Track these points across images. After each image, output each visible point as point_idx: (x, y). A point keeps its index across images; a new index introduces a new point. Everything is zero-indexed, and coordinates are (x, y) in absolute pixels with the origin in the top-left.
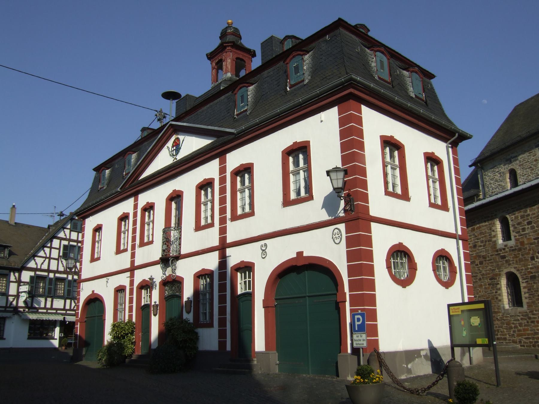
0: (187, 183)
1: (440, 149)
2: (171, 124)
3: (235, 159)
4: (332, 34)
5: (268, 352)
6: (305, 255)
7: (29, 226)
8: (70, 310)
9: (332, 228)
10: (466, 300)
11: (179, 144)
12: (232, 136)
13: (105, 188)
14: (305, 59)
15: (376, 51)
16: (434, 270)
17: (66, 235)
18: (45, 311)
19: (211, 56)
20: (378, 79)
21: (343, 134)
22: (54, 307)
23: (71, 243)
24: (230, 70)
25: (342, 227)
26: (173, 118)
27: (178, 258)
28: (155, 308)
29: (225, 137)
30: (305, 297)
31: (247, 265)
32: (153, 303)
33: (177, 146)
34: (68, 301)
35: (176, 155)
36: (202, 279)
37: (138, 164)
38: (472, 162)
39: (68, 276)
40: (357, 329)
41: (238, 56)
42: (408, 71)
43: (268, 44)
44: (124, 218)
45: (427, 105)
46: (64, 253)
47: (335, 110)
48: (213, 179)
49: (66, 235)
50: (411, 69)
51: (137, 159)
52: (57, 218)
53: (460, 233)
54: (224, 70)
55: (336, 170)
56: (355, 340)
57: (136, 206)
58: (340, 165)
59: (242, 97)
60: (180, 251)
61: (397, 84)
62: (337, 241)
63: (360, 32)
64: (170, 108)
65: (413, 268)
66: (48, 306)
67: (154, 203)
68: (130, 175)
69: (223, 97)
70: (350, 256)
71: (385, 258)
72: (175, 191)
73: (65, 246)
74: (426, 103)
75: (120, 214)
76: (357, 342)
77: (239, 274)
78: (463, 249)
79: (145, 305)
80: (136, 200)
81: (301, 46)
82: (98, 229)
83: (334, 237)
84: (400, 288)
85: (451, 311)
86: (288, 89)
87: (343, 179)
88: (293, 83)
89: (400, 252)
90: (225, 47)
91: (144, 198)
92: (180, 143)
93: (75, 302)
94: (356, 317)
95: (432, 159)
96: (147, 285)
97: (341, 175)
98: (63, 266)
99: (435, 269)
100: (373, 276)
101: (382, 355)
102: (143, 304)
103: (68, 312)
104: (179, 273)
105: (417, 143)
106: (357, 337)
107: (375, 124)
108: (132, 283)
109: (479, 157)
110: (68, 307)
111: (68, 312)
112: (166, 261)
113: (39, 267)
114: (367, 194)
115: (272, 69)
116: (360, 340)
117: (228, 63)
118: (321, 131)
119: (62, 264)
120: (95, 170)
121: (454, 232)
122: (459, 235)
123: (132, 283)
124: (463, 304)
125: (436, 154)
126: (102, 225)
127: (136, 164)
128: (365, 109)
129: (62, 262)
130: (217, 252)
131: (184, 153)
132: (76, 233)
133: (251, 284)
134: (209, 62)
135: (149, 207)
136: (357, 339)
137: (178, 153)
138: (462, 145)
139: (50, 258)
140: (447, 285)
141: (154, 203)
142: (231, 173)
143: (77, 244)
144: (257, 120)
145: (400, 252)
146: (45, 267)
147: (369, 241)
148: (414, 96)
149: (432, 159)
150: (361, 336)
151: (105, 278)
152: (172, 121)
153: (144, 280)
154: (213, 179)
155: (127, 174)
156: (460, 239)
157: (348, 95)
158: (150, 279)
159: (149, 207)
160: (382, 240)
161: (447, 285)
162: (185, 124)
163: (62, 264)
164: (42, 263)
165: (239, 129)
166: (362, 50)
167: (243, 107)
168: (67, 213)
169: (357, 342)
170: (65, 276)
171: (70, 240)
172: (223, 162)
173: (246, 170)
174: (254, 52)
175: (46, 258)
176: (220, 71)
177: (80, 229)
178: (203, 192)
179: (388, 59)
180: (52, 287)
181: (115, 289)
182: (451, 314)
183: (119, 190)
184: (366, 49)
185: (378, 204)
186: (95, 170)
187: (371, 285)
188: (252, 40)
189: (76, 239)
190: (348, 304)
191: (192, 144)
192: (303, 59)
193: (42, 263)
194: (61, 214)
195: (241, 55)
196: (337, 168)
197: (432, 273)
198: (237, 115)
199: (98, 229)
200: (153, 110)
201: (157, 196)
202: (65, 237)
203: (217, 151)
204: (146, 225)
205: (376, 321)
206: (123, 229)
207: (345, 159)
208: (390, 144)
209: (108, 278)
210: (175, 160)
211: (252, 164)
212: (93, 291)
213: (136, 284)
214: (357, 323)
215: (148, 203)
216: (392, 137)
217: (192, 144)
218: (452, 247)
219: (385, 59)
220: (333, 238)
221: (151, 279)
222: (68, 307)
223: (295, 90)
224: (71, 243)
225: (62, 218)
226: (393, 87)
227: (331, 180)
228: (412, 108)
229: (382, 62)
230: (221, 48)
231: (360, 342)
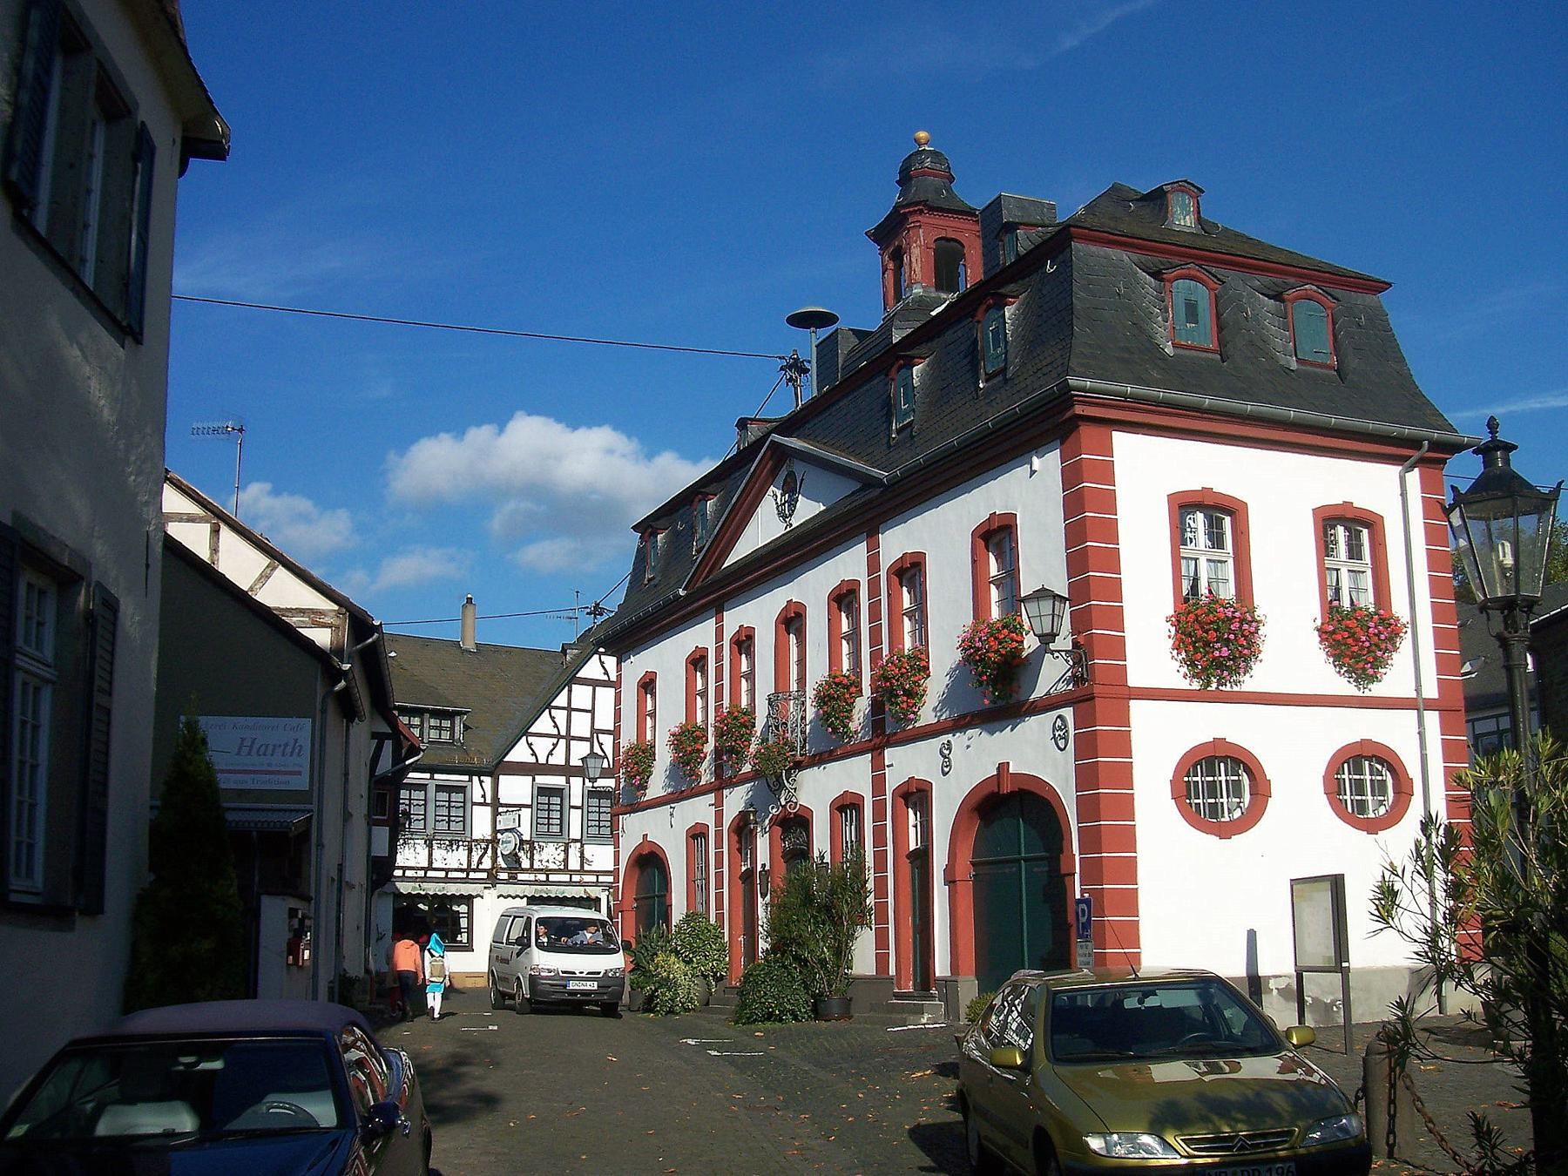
0: (812, 588)
3: (895, 542)
7: (509, 650)
17: (606, 673)
18: (566, 878)
22: (611, 868)
24: (919, 277)
30: (1018, 861)
49: (606, 673)
51: (718, 512)
52: (587, 623)
66: (574, 864)
70: (1086, 777)
91: (734, 619)
104: (804, 799)
108: (719, 816)
110: (574, 864)
113: (542, 760)
118: (1030, 491)
139: (569, 738)
146: (558, 759)
147: (1123, 744)
159: (744, 642)
164: (551, 753)
172: (873, 548)
175: (559, 736)
183: (682, 592)
190: (1077, 877)
193: (551, 753)
194: (597, 610)
198: (899, 431)
201: (758, 613)
225: (600, 619)
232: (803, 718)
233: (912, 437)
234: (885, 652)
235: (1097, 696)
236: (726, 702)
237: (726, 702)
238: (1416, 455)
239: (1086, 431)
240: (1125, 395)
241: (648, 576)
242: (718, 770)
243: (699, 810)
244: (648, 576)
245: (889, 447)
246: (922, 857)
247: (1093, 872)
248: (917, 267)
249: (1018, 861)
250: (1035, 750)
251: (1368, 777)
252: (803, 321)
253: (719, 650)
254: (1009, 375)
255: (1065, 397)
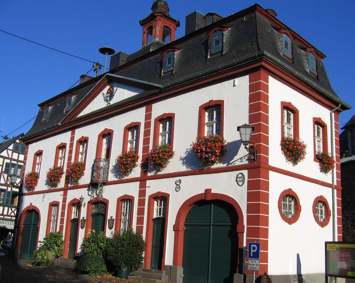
0: (118, 124)
1: (325, 114)
2: (107, 76)
3: (160, 108)
4: (248, 16)
5: (174, 266)
6: (212, 192)
8: (7, 215)
9: (237, 172)
10: (336, 240)
11: (112, 92)
12: (157, 91)
13: (47, 121)
14: (224, 34)
15: (282, 33)
16: (314, 212)
17: (8, 155)
19: (143, 23)
20: (282, 56)
21: (252, 98)
23: (13, 162)
24: (158, 35)
25: (245, 172)
26: (109, 71)
27: (105, 183)
28: (83, 222)
29: (152, 91)
30: (31, 224)
31: (163, 195)
32: (81, 218)
33: (111, 94)
34: (6, 208)
35: (110, 100)
36: (124, 203)
37: (77, 105)
38: (344, 125)
39: (7, 188)
40: (252, 255)
41: (166, 25)
42: (306, 51)
43: (191, 18)
44: (62, 147)
45: (319, 80)
46: (6, 169)
47: (246, 78)
48: (140, 123)
49: (8, 155)
50: (308, 49)
51: (77, 100)
53: (335, 184)
54: (153, 35)
55: (245, 126)
56: (250, 264)
57: (72, 139)
58: (248, 123)
59: (169, 59)
60: (107, 178)
61: (295, 61)
62: (240, 183)
63: (269, 15)
64: (106, 60)
65: (298, 208)
67: (88, 138)
68: (70, 112)
69: (153, 57)
70: (251, 197)
71: (278, 200)
72: (106, 129)
73: (7, 164)
74: (317, 77)
75: (59, 143)
76: (251, 266)
77: (156, 202)
78: (337, 197)
79: (74, 219)
80: (73, 134)
81: (221, 24)
82: (39, 154)
83: (238, 180)
84: (287, 224)
85: (328, 248)
86: (209, 57)
87: (251, 134)
88: (213, 52)
89: (289, 196)
90: (156, 17)
91: (80, 133)
92: (113, 91)
93: (11, 210)
94: (252, 246)
95: (318, 123)
96: (77, 204)
97: (249, 130)
98: (5, 180)
99: (315, 211)
100: (268, 213)
101: (270, 277)
102: (73, 218)
103: (5, 217)
105: (309, 109)
106: (252, 262)
107: (278, 92)
108: (65, 200)
109: (349, 122)
110: (5, 213)
111: (5, 217)
112: (94, 185)
114: (268, 148)
115: (195, 39)
116: (254, 265)
117: (158, 30)
118: (234, 94)
119: (4, 178)
120: (39, 105)
121: (331, 183)
122: (335, 186)
123: (65, 200)
124: (334, 242)
125: (322, 119)
126: (42, 151)
127: (75, 105)
128: (271, 79)
129: (3, 176)
130: (138, 183)
131: (115, 100)
132: (18, 154)
133: (165, 211)
134: (141, 27)
135: (84, 141)
136: (252, 263)
137: (111, 99)
138: (344, 112)
140: (323, 224)
141: (88, 138)
142: (155, 120)
143: (17, 163)
144: (182, 80)
145: (289, 196)
147: (266, 186)
148: (309, 72)
149: (318, 123)
150: (255, 262)
151: (43, 194)
152: (108, 72)
153: (75, 199)
154: (140, 123)
155: (67, 112)
156: (335, 189)
157: (253, 65)
158: (80, 198)
159: (84, 141)
160: (277, 185)
161: (323, 224)
162: (119, 76)
163: (4, 178)
165: (166, 85)
166: (272, 31)
167: (170, 67)
168: (11, 137)
169: (251, 266)
170: (5, 188)
171: (12, 159)
173: (168, 119)
174: (179, 22)
176: (149, 35)
177: (24, 152)
178: (130, 133)
179: (292, 40)
180: (6, 198)
181: (50, 203)
182: (328, 249)
183: (59, 124)
184: (275, 31)
185: (276, 156)
186: (39, 105)
187: (266, 221)
188: (179, 13)
189: (17, 158)
190: (245, 234)
191: (122, 94)
192: (223, 34)
194: (6, 138)
195: (169, 24)
196: (246, 125)
197: (312, 214)
199: (39, 154)
200: (91, 62)
202: (8, 156)
203: (145, 100)
204: (80, 155)
205: (267, 250)
206: (60, 156)
207: (252, 118)
208: (288, 108)
209: (44, 194)
210: (108, 105)
211: (174, 115)
212: (31, 204)
213: (68, 201)
214: (252, 251)
215: (83, 137)
216: (290, 103)
217: (122, 94)
218: (328, 194)
219: (289, 40)
220: (237, 181)
221: (82, 199)
222: (5, 213)
223: (214, 58)
224: (13, 162)
225: (6, 140)
226: (293, 63)
227: (241, 134)
228: (308, 81)
229: (286, 44)
230: (152, 17)
231: (253, 266)
232: (108, 168)
233: (172, 75)
234: (151, 148)
235: (257, 168)
236: (73, 161)
237: (73, 161)
238: (336, 108)
239: (262, 72)
240: (276, 62)
241: (43, 120)
242: (67, 183)
243: (57, 197)
244: (43, 120)
245: (160, 78)
246: (162, 222)
247: (254, 232)
248: (158, 32)
249: (210, 226)
250: (226, 184)
251: (319, 208)
252: (103, 51)
253: (71, 145)
254: (223, 53)
255: (261, 57)
